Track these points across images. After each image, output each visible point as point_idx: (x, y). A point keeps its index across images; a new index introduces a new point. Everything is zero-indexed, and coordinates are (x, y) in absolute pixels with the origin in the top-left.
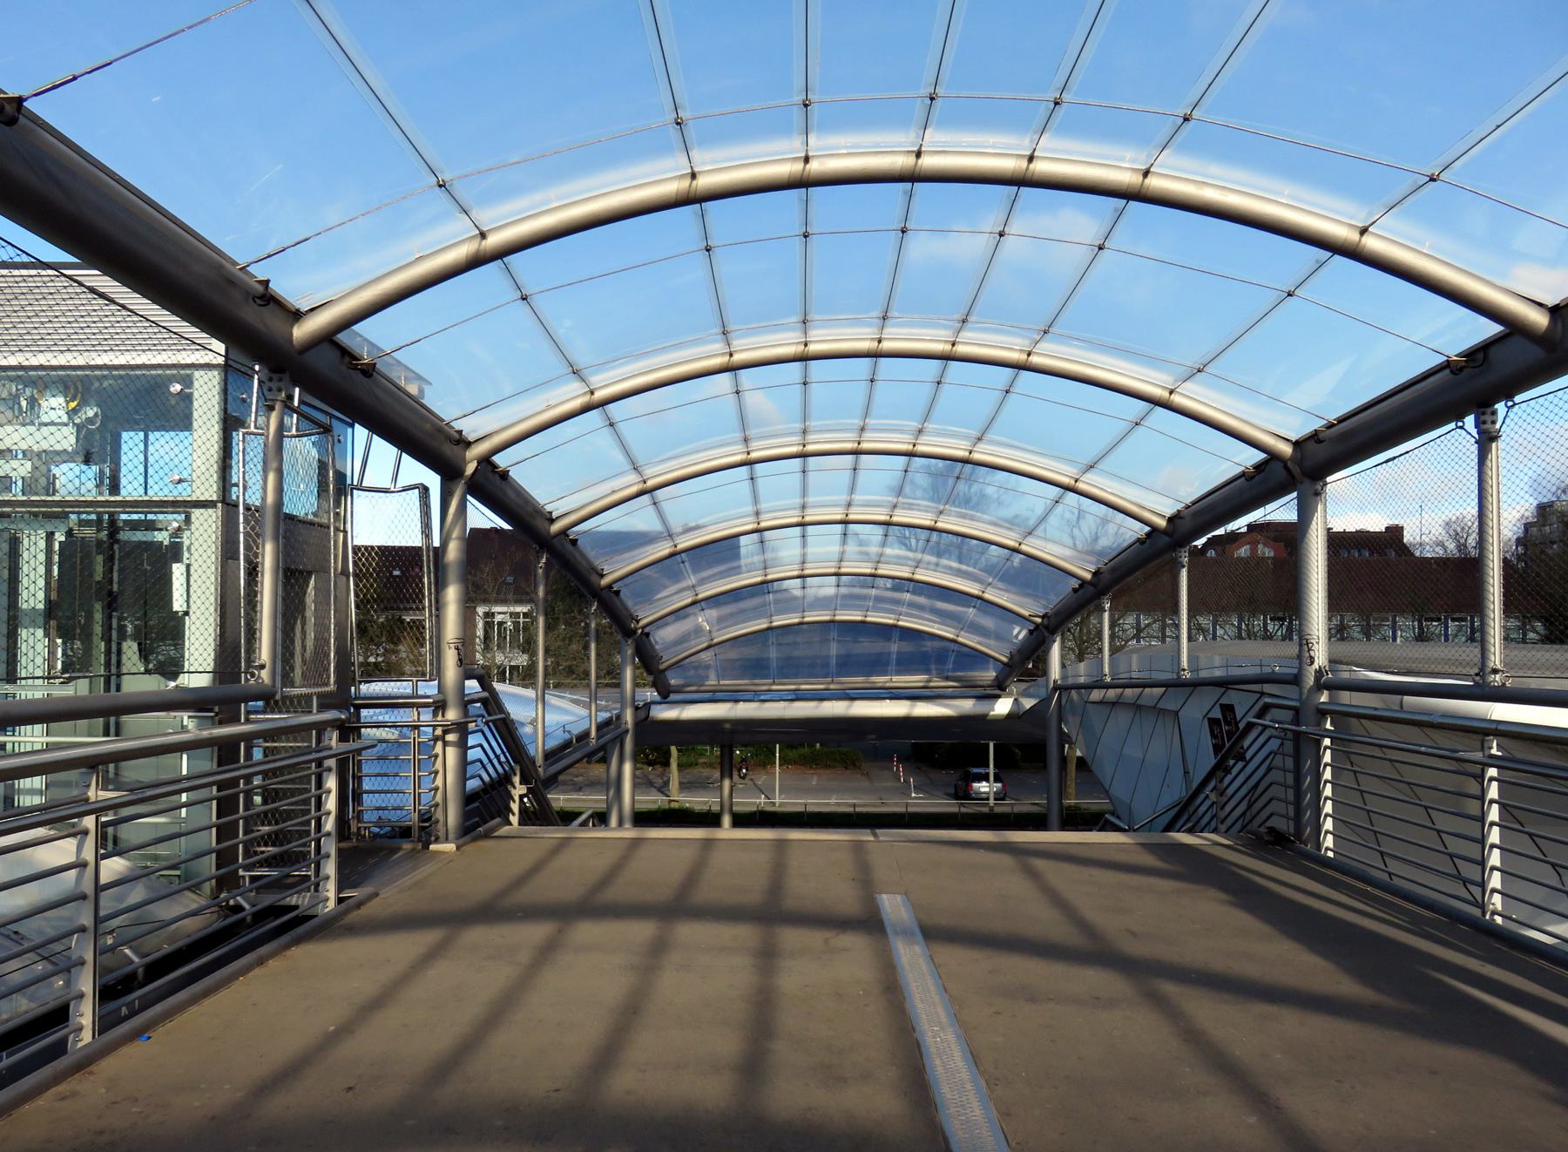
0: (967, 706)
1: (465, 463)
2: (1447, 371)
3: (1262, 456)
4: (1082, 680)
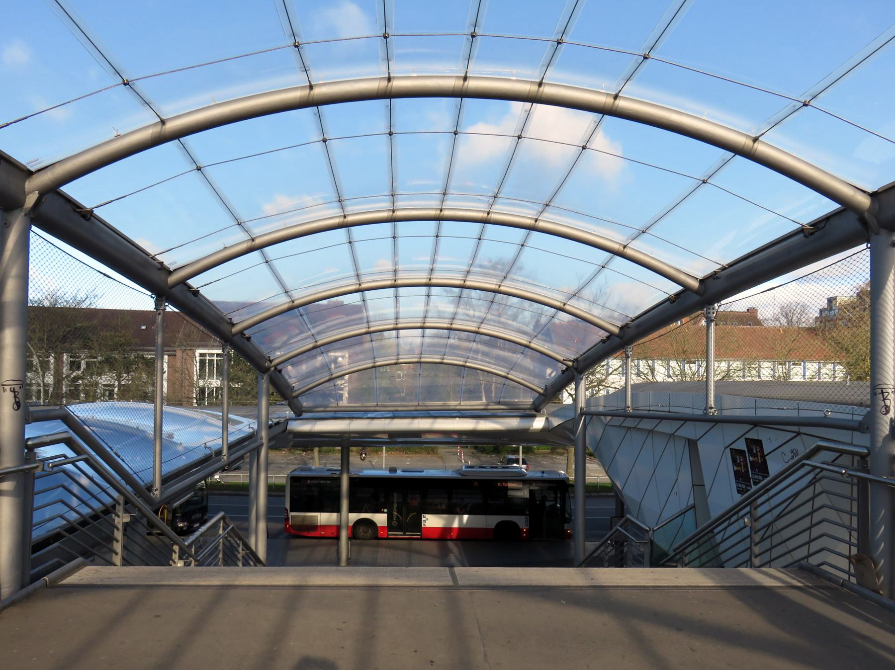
0: (513, 423)
1: (24, 194)
2: (802, 235)
3: (680, 288)
4: (601, 409)
